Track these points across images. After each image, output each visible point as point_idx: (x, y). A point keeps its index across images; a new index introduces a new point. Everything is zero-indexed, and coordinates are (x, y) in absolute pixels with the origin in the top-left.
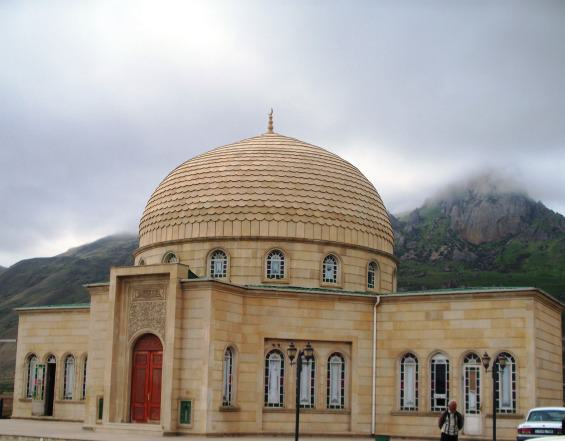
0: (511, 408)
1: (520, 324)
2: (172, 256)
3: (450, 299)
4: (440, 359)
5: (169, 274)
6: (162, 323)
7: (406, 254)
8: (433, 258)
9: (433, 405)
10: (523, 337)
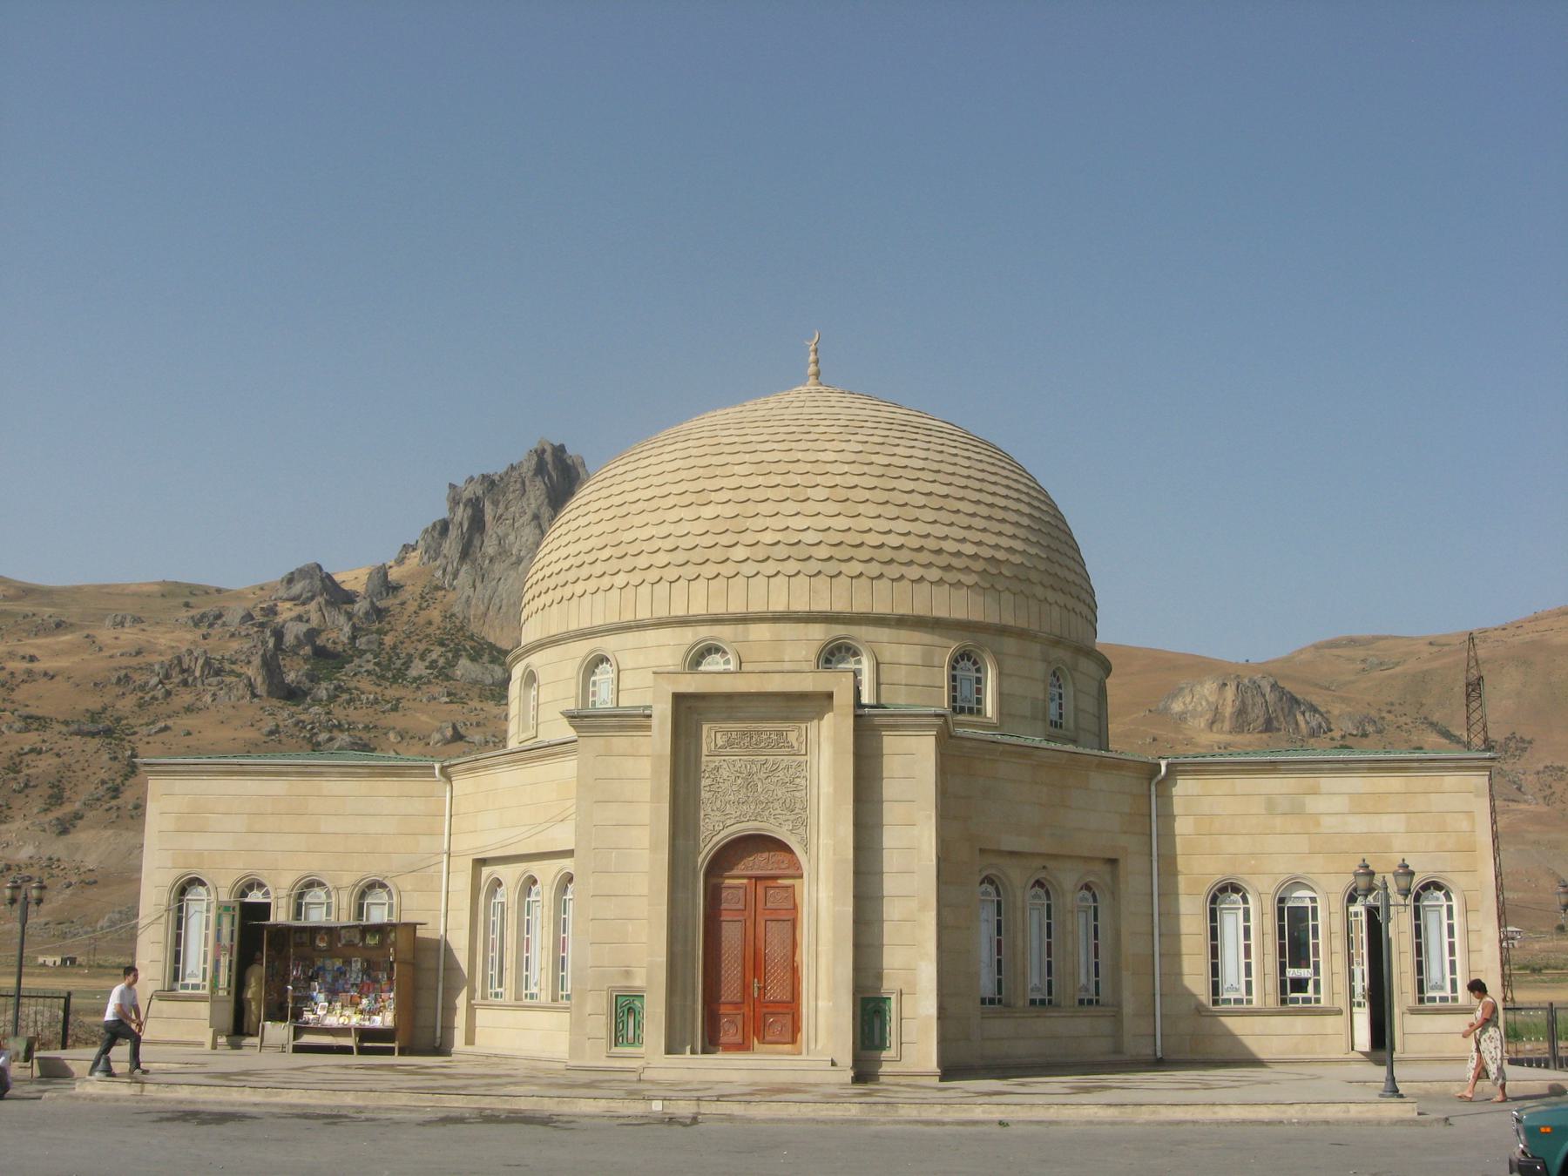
0: (1448, 992)
1: (1464, 825)
2: (603, 659)
3: (1321, 770)
4: (1301, 897)
5: (830, 696)
6: (799, 812)
7: (357, 661)
8: (413, 673)
9: (1283, 991)
10: (1471, 850)
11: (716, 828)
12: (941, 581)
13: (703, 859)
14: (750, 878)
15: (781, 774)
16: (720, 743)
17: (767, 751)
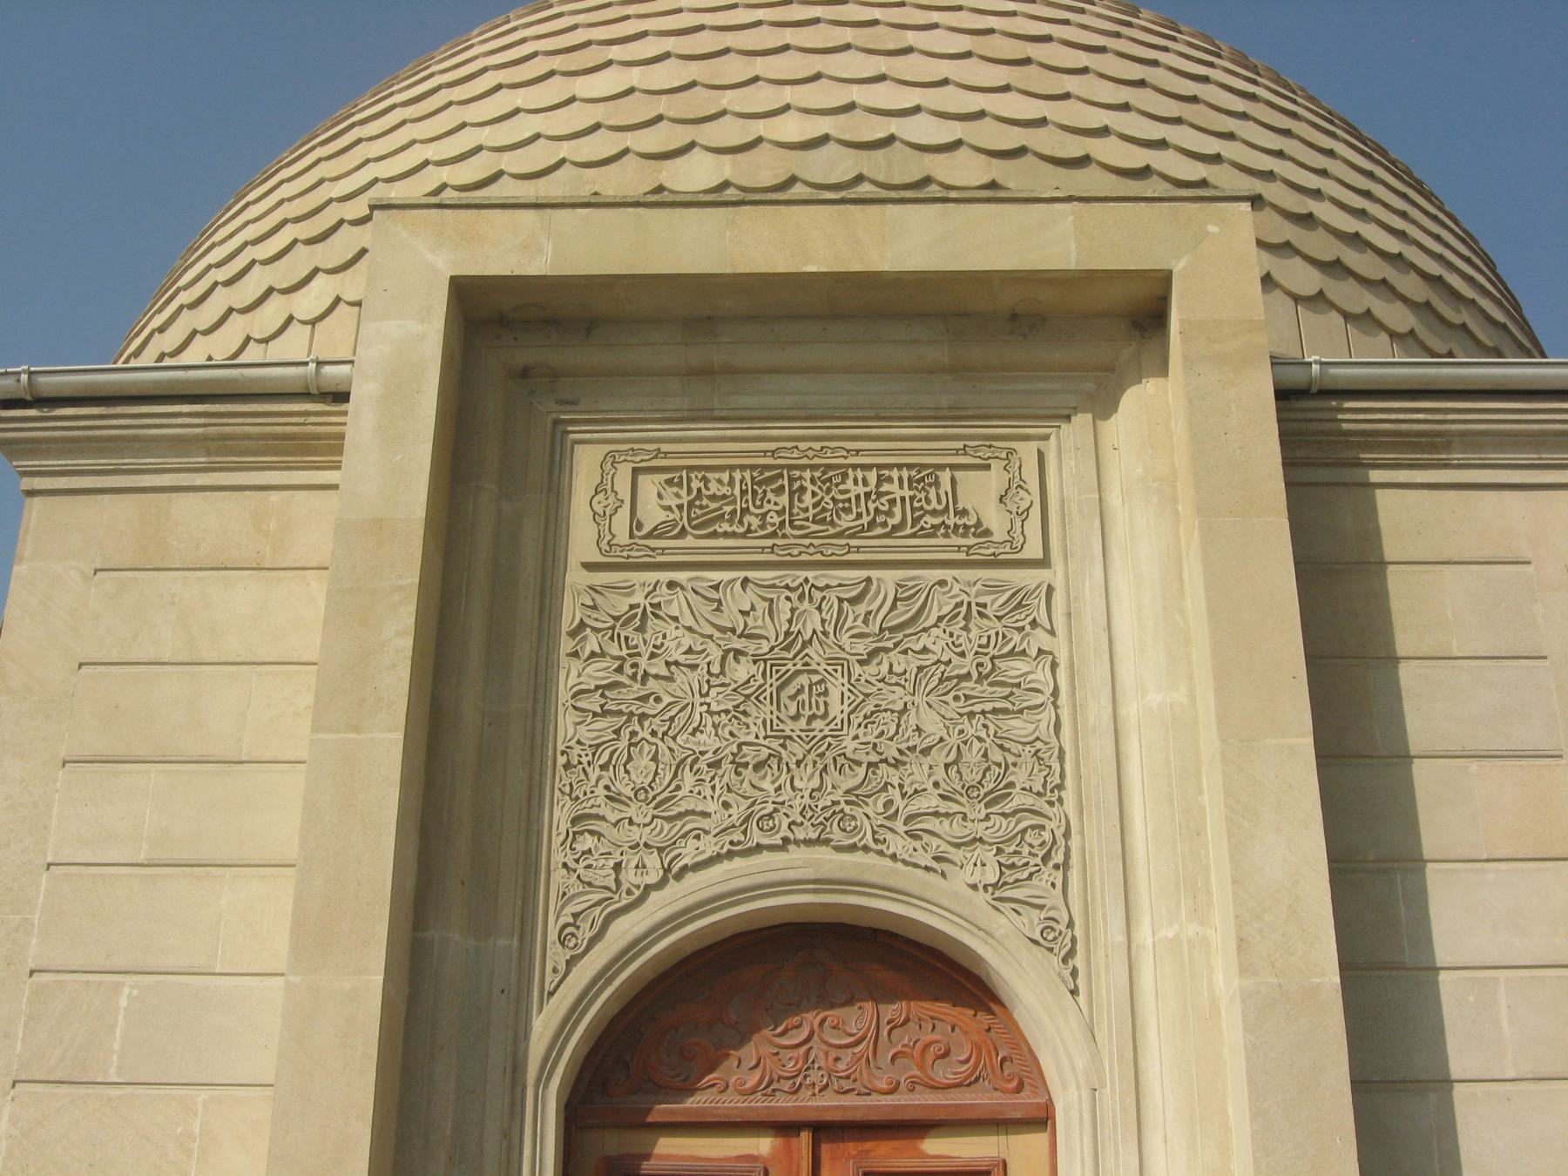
11: (625, 883)
12: (1318, 300)
13: (555, 1022)
14: (784, 1128)
15: (937, 642)
16: (652, 514)
17: (872, 546)
